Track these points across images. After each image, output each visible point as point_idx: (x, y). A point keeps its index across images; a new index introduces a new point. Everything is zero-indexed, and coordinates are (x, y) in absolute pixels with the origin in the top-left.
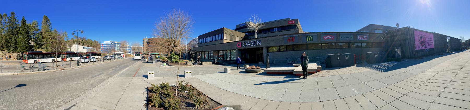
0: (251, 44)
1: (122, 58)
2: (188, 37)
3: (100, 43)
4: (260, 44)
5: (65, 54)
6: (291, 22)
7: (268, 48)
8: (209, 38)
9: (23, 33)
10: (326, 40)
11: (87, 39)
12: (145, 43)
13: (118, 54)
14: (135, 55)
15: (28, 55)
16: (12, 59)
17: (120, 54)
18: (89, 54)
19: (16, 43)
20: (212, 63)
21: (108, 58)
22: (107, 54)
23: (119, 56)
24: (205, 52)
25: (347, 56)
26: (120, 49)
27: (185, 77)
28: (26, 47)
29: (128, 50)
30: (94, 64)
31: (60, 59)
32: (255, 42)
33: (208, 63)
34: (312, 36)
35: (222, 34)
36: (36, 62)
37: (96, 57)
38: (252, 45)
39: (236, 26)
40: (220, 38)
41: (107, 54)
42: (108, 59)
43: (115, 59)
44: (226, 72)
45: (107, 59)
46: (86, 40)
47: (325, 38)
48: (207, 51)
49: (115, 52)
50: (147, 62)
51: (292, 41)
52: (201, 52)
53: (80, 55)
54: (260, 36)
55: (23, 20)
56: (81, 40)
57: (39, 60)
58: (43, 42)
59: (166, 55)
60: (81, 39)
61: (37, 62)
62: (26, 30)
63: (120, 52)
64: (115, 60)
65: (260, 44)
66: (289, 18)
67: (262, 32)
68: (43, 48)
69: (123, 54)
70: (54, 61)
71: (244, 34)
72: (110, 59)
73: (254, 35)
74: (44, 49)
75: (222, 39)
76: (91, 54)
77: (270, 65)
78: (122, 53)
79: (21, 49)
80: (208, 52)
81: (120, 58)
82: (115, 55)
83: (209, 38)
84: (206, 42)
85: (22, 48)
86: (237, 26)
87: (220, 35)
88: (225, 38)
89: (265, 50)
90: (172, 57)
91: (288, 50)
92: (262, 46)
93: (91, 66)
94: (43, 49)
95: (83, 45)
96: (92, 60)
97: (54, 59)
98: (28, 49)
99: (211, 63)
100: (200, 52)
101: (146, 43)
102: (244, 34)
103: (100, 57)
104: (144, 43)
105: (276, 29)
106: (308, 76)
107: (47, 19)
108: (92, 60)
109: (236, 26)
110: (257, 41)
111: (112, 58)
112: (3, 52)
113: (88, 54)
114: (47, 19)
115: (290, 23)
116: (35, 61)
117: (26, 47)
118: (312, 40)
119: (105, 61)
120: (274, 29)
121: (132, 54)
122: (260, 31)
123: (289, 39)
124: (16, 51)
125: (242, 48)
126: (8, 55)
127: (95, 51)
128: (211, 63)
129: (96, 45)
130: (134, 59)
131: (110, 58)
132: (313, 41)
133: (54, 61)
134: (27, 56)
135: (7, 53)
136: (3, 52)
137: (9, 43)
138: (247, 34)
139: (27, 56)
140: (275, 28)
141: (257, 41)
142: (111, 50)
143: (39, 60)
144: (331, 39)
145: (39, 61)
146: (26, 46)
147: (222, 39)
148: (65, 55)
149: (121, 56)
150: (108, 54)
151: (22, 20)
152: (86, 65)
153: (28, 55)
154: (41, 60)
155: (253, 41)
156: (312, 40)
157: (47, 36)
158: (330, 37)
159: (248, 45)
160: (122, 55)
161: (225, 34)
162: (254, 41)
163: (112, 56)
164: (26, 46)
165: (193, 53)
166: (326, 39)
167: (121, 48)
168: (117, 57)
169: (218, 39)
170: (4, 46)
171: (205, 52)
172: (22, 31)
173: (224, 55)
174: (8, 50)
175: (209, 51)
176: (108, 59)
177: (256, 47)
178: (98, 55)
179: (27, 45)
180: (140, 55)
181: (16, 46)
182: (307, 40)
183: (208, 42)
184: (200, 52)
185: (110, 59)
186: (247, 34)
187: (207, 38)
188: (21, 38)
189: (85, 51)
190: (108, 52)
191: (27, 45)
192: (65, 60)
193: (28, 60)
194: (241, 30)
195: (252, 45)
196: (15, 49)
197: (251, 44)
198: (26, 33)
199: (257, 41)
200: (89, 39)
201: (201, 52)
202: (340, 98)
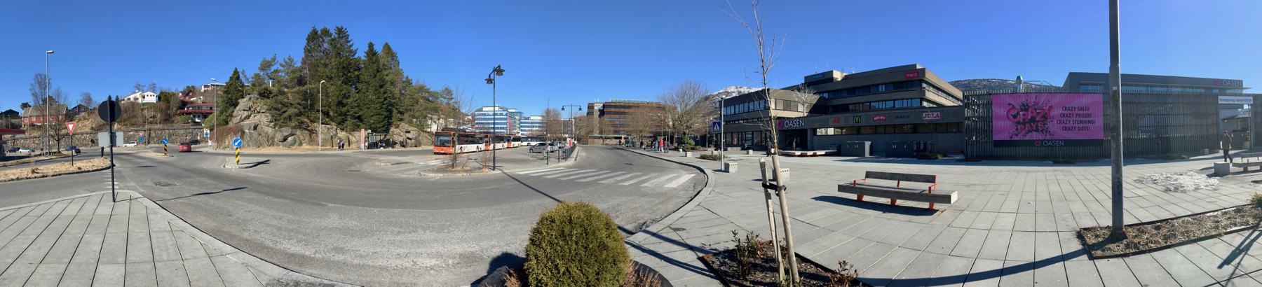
6: (912, 75)
8: (741, 106)
24: (732, 133)
25: (856, 144)
27: (387, 44)
33: (735, 148)
48: (891, 100)
66: (916, 65)
67: (857, 93)
79: (372, 121)
80: (893, 102)
86: (806, 78)
88: (772, 106)
91: (897, 131)
92: (806, 127)
99: (740, 148)
101: (596, 114)
102: (817, 97)
105: (884, 86)
112: (328, 129)
115: (909, 77)
120: (880, 87)
125: (784, 129)
128: (740, 148)
136: (328, 129)
137: (344, 105)
138: (826, 95)
140: (882, 84)
158: (881, 118)
171: (732, 133)
186: (826, 95)
196: (359, 122)
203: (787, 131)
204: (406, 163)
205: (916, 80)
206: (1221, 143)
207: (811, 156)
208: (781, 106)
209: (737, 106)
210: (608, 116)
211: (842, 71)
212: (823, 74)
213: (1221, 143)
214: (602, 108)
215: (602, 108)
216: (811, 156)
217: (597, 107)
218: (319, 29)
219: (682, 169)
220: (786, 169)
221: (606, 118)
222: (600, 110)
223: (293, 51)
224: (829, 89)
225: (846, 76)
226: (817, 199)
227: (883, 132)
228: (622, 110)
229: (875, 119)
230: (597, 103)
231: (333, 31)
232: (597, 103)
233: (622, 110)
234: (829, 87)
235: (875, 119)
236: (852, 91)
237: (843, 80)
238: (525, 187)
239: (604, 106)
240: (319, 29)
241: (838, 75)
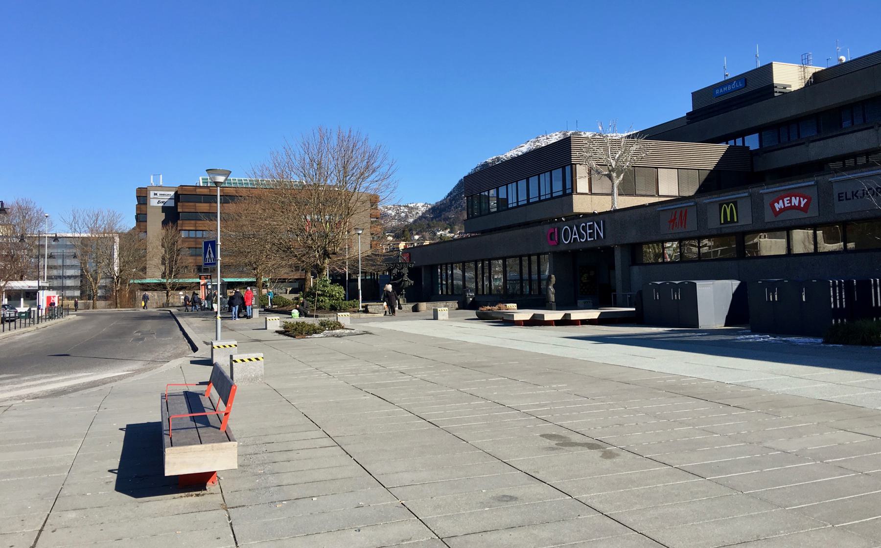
0: (581, 237)
2: (363, 230)
10: (781, 217)
20: (457, 306)
34: (735, 203)
35: (568, 169)
40: (558, 187)
44: (435, 318)
47: (776, 205)
51: (682, 225)
52: (538, 255)
59: (296, 285)
63: (33, 284)
67: (846, 124)
75: (569, 190)
77: (557, 305)
78: (43, 288)
83: (542, 176)
84: (529, 203)
86: (696, 96)
87: (557, 173)
88: (582, 185)
92: (609, 242)
99: (455, 304)
100: (534, 258)
101: (155, 220)
106: (298, 287)
109: (692, 93)
118: (735, 220)
123: (673, 218)
125: (561, 248)
128: (455, 304)
132: (737, 222)
144: (798, 208)
156: (735, 220)
158: (795, 201)
159: (573, 237)
161: (581, 171)
162: (588, 224)
165: (404, 274)
166: (781, 209)
169: (552, 193)
173: (521, 279)
175: (520, 257)
182: (722, 222)
183: (552, 198)
184: (534, 258)
186: (752, 142)
187: (533, 181)
197: (581, 237)
199: (594, 223)
201: (538, 255)
203: (564, 253)
206: (856, 300)
207: (558, 323)
209: (523, 198)
211: (804, 62)
212: (744, 78)
213: (856, 300)
214: (172, 204)
215: (172, 204)
216: (558, 323)
217: (155, 201)
220: (253, 356)
221: (185, 232)
222: (165, 209)
224: (761, 121)
225: (814, 74)
228: (684, 224)
229: (778, 206)
230: (161, 188)
232: (161, 188)
233: (684, 224)
234: (763, 113)
235: (778, 206)
238: (65, 354)
239: (177, 197)
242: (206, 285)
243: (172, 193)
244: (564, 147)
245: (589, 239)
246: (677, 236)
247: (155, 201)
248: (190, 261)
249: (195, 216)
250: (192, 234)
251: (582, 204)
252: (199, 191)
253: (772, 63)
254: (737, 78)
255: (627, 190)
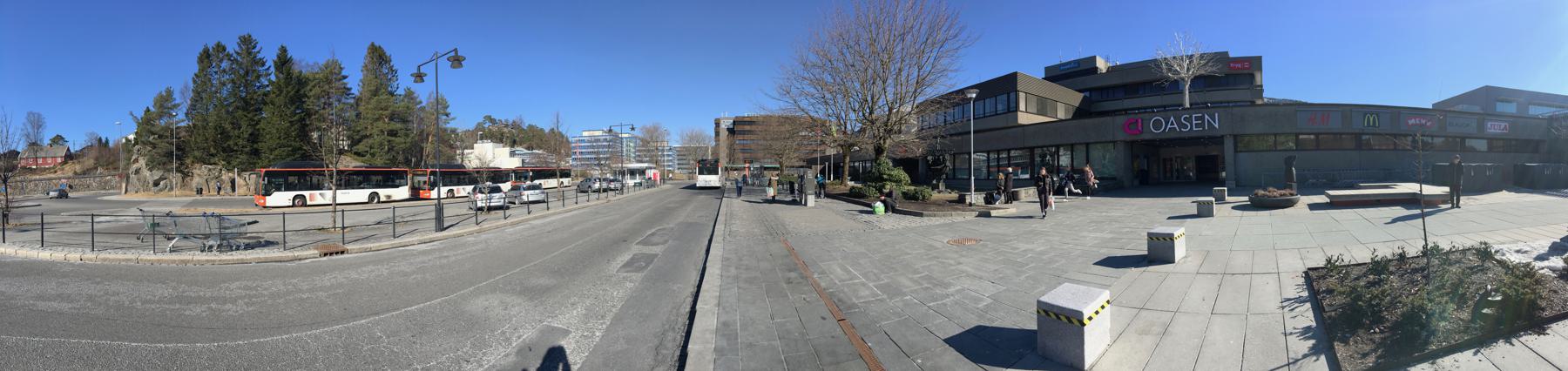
0: (1181, 125)
1: (651, 183)
3: (570, 139)
4: (1217, 126)
5: (426, 175)
6: (1240, 66)
7: (1235, 137)
9: (280, 101)
11: (527, 125)
12: (721, 134)
13: (633, 173)
14: (701, 173)
15: (266, 179)
16: (241, 190)
17: (642, 172)
18: (525, 174)
19: (254, 138)
21: (597, 185)
22: (592, 172)
23: (638, 179)
26: (639, 156)
28: (290, 149)
29: (666, 158)
30: (531, 216)
31: (403, 192)
32: (1197, 119)
35: (1012, 95)
36: (300, 203)
37: (552, 183)
38: (1186, 126)
39: (1046, 68)
41: (592, 172)
42: (598, 191)
43: (625, 190)
45: (593, 189)
46: (524, 130)
49: (624, 165)
50: (773, 201)
53: (498, 175)
54: (1200, 98)
55: (279, 57)
56: (505, 130)
57: (458, 190)
58: (359, 131)
60: (507, 126)
61: (304, 205)
62: (293, 92)
64: (624, 195)
65: (1217, 126)
67: (1141, 93)
68: (356, 153)
69: (653, 171)
70: (376, 200)
71: (1081, 96)
72: (605, 191)
73: (1182, 93)
74: (363, 156)
76: (531, 173)
78: (651, 168)
81: (641, 184)
82: (623, 173)
85: (276, 152)
86: (1047, 69)
88: (1022, 106)
89: (1229, 145)
90: (885, 177)
93: (511, 230)
94: (356, 157)
95: (514, 143)
96: (529, 195)
97: (377, 194)
98: (296, 156)
101: (724, 134)
102: (1081, 96)
103: (566, 181)
104: (717, 134)
107: (380, 56)
108: (529, 195)
109: (1046, 68)
110: (1206, 116)
111: (612, 186)
112: (210, 170)
113: (519, 174)
114: (380, 56)
115: (1234, 68)
116: (295, 197)
117: (290, 149)
119: (582, 197)
121: (679, 169)
122: (1200, 82)
124: (254, 164)
126: (226, 176)
127: (553, 162)
129: (554, 141)
130: (693, 187)
131: (605, 185)
133: (376, 200)
134: (264, 180)
135: (223, 172)
139: (264, 180)
141: (1206, 116)
142: (607, 159)
143: (312, 197)
145: (311, 200)
146: (291, 146)
147: (1009, 111)
148: (426, 179)
149: (647, 177)
150: (596, 173)
151: (276, 59)
152: (485, 225)
153: (266, 179)
154: (319, 197)
155: (1191, 117)
157: (372, 109)
159: (1169, 126)
160: (650, 173)
161: (1022, 96)
163: (612, 178)
164: (291, 146)
167: (639, 151)
168: (630, 182)
170: (212, 149)
172: (277, 96)
174: (229, 163)
175: (988, 153)
176: (598, 191)
177: (1200, 135)
178: (556, 175)
179: (293, 143)
180: (717, 174)
181: (255, 146)
185: (605, 191)
188: (272, 121)
189: (514, 163)
190: (599, 165)
191: (293, 143)
192: (426, 195)
193: (267, 197)
194: (1070, 80)
195: (1186, 126)
197: (1181, 125)
198: (292, 101)
200: (531, 127)
202: (1201, 271)
204: (1031, 217)
205: (1245, 74)
208: (1033, 108)
210: (741, 137)
212: (1078, 62)
214: (732, 127)
217: (724, 125)
218: (211, 46)
219: (701, 194)
221: (738, 140)
223: (180, 78)
226: (1169, 218)
227: (1320, 137)
231: (232, 47)
234: (1090, 82)
236: (1132, 89)
237: (1108, 71)
240: (211, 46)
241: (1102, 65)
242: (749, 168)
243: (732, 121)
244: (1012, 78)
245: (1194, 129)
246: (1316, 131)
247: (724, 125)
248: (740, 156)
249: (743, 132)
250: (742, 142)
251: (1024, 118)
252: (745, 119)
253: (1095, 57)
254: (1074, 62)
255: (1041, 112)
